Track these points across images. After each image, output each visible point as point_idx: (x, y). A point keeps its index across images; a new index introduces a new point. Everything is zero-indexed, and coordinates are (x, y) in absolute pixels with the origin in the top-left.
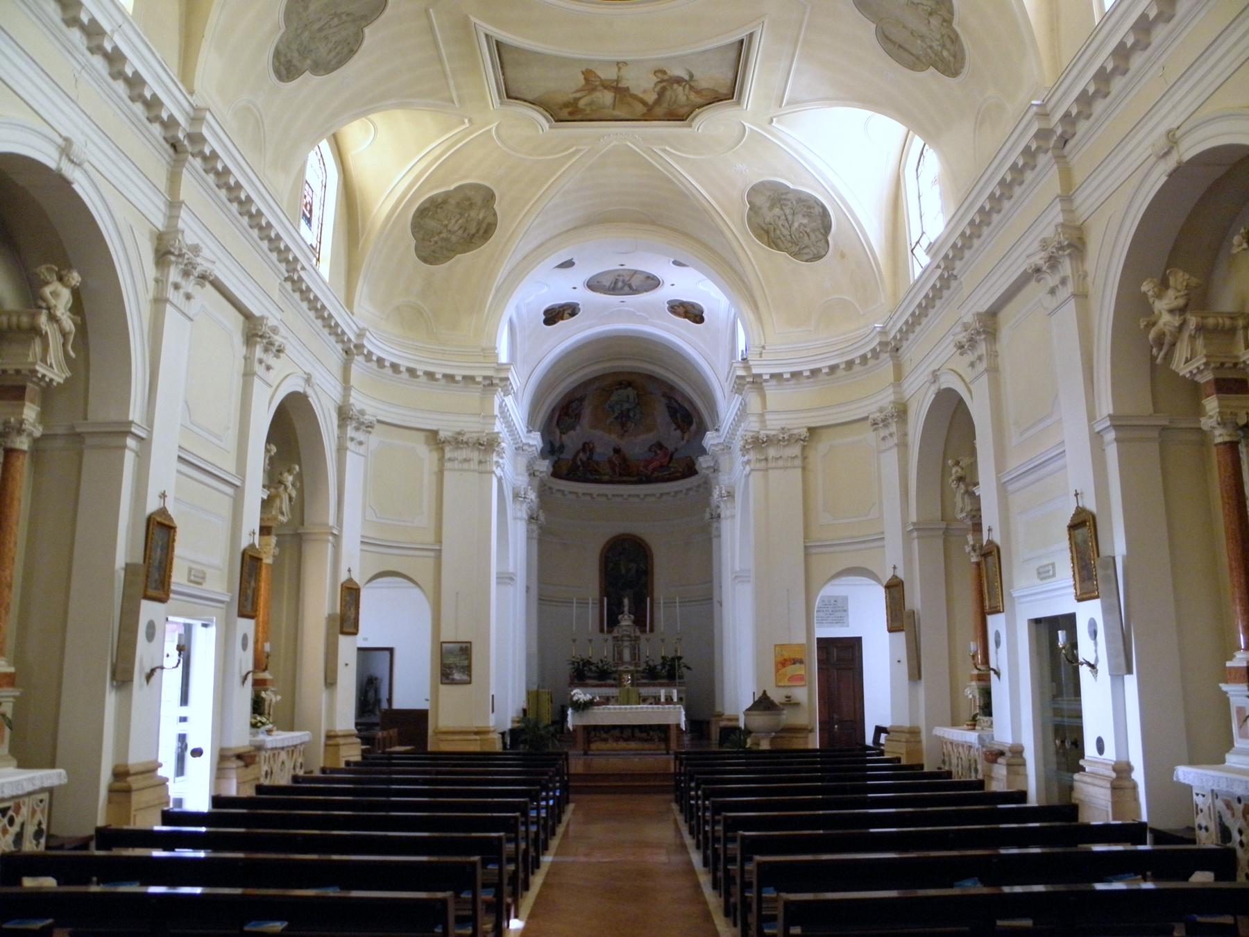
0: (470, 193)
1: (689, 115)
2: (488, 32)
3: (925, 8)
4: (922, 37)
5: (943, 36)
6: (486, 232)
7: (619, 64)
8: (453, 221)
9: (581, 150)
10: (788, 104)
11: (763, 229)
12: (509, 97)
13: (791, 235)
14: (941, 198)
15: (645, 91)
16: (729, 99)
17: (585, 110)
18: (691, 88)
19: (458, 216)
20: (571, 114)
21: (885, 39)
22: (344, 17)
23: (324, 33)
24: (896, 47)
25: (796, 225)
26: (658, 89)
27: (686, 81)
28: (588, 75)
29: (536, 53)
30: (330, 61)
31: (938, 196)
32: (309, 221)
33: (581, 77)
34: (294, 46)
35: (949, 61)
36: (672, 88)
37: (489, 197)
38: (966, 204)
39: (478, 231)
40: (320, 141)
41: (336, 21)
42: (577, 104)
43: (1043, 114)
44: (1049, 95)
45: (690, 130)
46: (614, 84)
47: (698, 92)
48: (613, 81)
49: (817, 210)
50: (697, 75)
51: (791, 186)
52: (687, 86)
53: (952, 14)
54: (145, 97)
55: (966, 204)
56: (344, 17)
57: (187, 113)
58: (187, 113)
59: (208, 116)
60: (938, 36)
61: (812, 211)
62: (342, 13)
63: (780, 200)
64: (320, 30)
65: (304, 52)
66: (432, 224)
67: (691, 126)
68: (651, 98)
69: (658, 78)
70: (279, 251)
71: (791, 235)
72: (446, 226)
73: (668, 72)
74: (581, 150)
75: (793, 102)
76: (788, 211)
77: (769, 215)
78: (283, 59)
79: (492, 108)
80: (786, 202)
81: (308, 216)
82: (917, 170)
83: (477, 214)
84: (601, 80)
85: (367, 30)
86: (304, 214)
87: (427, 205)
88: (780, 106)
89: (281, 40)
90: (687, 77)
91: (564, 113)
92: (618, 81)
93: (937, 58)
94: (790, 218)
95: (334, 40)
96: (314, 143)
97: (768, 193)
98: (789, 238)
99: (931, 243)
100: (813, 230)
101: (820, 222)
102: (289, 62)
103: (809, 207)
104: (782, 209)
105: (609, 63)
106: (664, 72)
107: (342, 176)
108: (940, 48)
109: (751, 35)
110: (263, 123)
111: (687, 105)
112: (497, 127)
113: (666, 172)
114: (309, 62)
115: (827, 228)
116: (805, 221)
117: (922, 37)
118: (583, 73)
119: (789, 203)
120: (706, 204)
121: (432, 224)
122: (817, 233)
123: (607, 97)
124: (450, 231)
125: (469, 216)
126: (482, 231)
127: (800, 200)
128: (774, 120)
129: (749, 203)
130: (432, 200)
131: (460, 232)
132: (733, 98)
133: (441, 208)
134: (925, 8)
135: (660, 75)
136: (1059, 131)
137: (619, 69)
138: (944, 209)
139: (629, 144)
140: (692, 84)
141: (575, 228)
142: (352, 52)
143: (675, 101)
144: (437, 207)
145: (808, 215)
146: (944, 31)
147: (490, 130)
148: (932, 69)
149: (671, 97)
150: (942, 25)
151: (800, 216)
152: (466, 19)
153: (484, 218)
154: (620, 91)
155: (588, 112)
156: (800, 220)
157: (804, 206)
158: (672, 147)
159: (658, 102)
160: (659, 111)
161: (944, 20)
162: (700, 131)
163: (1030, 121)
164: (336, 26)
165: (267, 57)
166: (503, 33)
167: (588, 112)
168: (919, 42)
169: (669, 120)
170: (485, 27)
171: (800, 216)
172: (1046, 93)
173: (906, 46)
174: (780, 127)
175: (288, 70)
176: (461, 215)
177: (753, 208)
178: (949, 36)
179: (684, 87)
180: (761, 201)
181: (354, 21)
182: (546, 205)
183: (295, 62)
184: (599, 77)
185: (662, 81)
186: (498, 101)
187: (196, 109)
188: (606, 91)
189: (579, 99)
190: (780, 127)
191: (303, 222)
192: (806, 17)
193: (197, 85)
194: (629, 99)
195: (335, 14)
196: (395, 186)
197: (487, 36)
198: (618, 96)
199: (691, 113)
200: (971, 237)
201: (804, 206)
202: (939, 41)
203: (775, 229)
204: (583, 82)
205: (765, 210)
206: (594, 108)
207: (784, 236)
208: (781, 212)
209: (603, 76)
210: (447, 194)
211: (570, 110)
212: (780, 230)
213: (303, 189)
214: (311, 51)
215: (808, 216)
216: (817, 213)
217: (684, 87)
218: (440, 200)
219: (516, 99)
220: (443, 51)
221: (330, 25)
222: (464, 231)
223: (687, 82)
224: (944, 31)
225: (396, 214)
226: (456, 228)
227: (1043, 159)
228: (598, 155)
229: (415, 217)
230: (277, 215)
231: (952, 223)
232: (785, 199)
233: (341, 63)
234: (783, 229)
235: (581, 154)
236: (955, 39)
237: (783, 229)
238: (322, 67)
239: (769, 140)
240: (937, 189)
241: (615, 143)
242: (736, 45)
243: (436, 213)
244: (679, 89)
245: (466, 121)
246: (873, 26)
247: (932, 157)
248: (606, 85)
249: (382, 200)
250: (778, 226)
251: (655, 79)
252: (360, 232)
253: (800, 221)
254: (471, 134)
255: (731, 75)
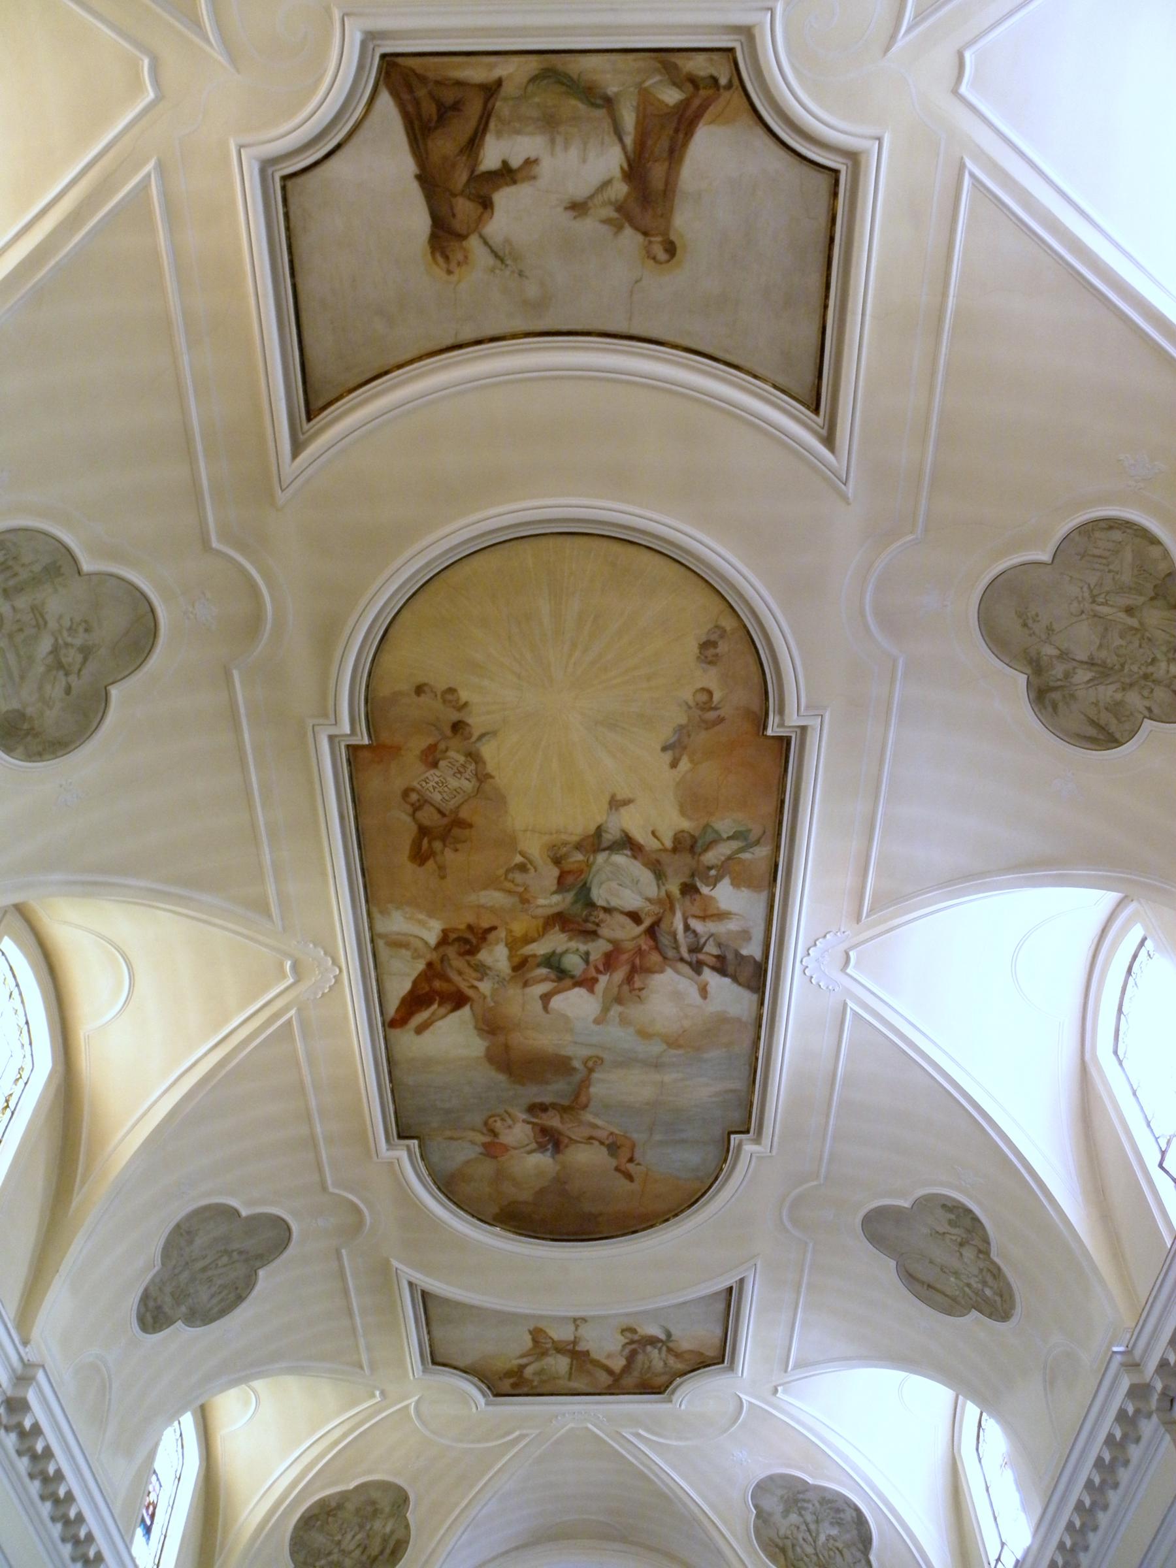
0: (375, 1495)
1: (668, 1387)
2: (413, 1280)
3: (954, 1238)
4: (956, 1274)
5: (981, 1270)
6: (393, 1553)
7: (577, 1321)
8: (349, 1536)
9: (527, 1435)
10: (796, 1367)
11: (777, 1546)
12: (434, 1363)
13: (816, 1554)
14: (1018, 1490)
15: (609, 1356)
16: (718, 1363)
17: (532, 1381)
18: (669, 1350)
19: (356, 1529)
20: (514, 1385)
21: (910, 1278)
22: (235, 1255)
23: (210, 1273)
24: (925, 1287)
25: (822, 1538)
26: (627, 1351)
27: (661, 1341)
28: (537, 1334)
29: (472, 1307)
30: (210, 1309)
31: (1014, 1487)
32: (148, 1530)
33: (528, 1339)
34: (168, 1289)
35: (995, 1301)
36: (644, 1351)
37: (400, 1499)
38: (1056, 1499)
39: (382, 1552)
40: (181, 1415)
41: (225, 1259)
42: (522, 1372)
43: (1132, 1365)
44: (1134, 1337)
45: (669, 1406)
46: (569, 1347)
47: (678, 1355)
48: (569, 1343)
49: (849, 1515)
50: (676, 1333)
51: (810, 1481)
52: (664, 1348)
53: (989, 1243)
54: (24, 1428)
55: (1056, 1499)
56: (235, 1255)
57: (13, 1370)
58: (13, 1370)
59: (41, 1376)
60: (976, 1272)
61: (842, 1515)
62: (233, 1251)
63: (796, 1501)
64: (204, 1269)
65: (179, 1296)
66: (318, 1539)
67: (671, 1401)
68: (618, 1364)
69: (626, 1338)
70: (77, 1542)
71: (816, 1554)
72: (339, 1543)
73: (639, 1330)
74: (527, 1435)
75: (801, 1365)
76: (809, 1518)
77: (785, 1524)
78: (151, 1304)
79: (412, 1378)
80: (806, 1505)
81: (148, 1522)
82: (977, 1450)
83: (383, 1526)
84: (553, 1342)
85: (261, 1273)
86: (143, 1520)
87: (316, 1511)
88: (786, 1371)
89: (152, 1281)
90: (663, 1337)
91: (506, 1385)
92: (575, 1342)
93: (979, 1299)
94: (813, 1527)
95: (219, 1282)
96: (175, 1415)
97: (780, 1492)
98: (814, 1558)
99: (1017, 1561)
100: (848, 1546)
101: (855, 1532)
102: (159, 1308)
103: (838, 1511)
104: (801, 1515)
105: (564, 1319)
106: (634, 1331)
107: (204, 1464)
108: (980, 1286)
109: (742, 1281)
110: (110, 1387)
111: (664, 1373)
112: (418, 1403)
113: (641, 1467)
114: (183, 1309)
115: (865, 1541)
116: (834, 1532)
117: (956, 1274)
118: (530, 1332)
119: (810, 1506)
120: (696, 1510)
121: (318, 1539)
122: (854, 1550)
123: (561, 1364)
124: (343, 1551)
125: (371, 1529)
126: (388, 1551)
127: (824, 1501)
128: (780, 1389)
129: (756, 1507)
130: (322, 1503)
131: (358, 1552)
132: (723, 1362)
133: (334, 1515)
134: (954, 1238)
135: (628, 1335)
136: (1159, 1386)
137: (577, 1327)
138: (1025, 1506)
139: (590, 1426)
140: (671, 1345)
141: (517, 1548)
142: (240, 1299)
143: (649, 1367)
144: (328, 1514)
145: (839, 1523)
146: (981, 1264)
147: (407, 1407)
148: (975, 1314)
149: (643, 1363)
150: (978, 1257)
151: (826, 1524)
152: (387, 1262)
153: (392, 1532)
154: (579, 1357)
155: (535, 1383)
156: (828, 1531)
157: (831, 1509)
158: (648, 1430)
159: (627, 1369)
160: (629, 1381)
161: (980, 1251)
162: (683, 1407)
163: (1116, 1377)
164: (225, 1266)
165: (134, 1298)
166: (437, 1284)
167: (535, 1383)
168: (952, 1279)
169: (641, 1394)
170: (409, 1273)
171: (826, 1524)
172: (1128, 1336)
173: (938, 1286)
174: (785, 1398)
175: (155, 1319)
176: (361, 1527)
177: (760, 1514)
178: (989, 1270)
179: (660, 1350)
180: (772, 1504)
181: (246, 1260)
182: (477, 1515)
183: (167, 1309)
184: (551, 1338)
185: (632, 1342)
186: (420, 1367)
187: (26, 1365)
188: (559, 1356)
189: (524, 1366)
190: (785, 1398)
191: (139, 1532)
192: (809, 1256)
193: (36, 1334)
194: (590, 1367)
195: (228, 1253)
196: (274, 1482)
197: (411, 1284)
198: (575, 1362)
199: (671, 1383)
200: (1073, 1550)
201: (831, 1509)
202: (976, 1276)
203: (793, 1546)
204: (530, 1344)
205: (777, 1517)
206: (544, 1378)
207: (806, 1555)
208: (801, 1520)
209: (555, 1337)
210: (344, 1496)
211: (512, 1380)
212: (801, 1547)
213: (148, 1482)
214: (189, 1295)
215: (838, 1523)
216: (849, 1519)
217: (660, 1350)
218: (333, 1504)
219: (444, 1365)
220: (355, 1304)
221: (217, 1265)
222: (363, 1553)
223: (664, 1343)
224: (981, 1264)
225: (270, 1524)
226: (352, 1547)
227: (1148, 1427)
228: (549, 1443)
229: (297, 1528)
230: (81, 1475)
231: (1042, 1527)
232: (804, 1500)
233: (224, 1312)
234: (805, 1545)
235: (527, 1440)
236: (996, 1273)
237: (805, 1545)
238: (200, 1317)
239: (776, 1416)
240: (1009, 1475)
241: (572, 1425)
242: (724, 1295)
243: (328, 1523)
244: (653, 1353)
245: (377, 1393)
246: (893, 1263)
247: (993, 1429)
248: (560, 1348)
249: (255, 1500)
250: (796, 1539)
251: (623, 1340)
252: (218, 1549)
253: (827, 1532)
254: (385, 1409)
255: (719, 1332)
